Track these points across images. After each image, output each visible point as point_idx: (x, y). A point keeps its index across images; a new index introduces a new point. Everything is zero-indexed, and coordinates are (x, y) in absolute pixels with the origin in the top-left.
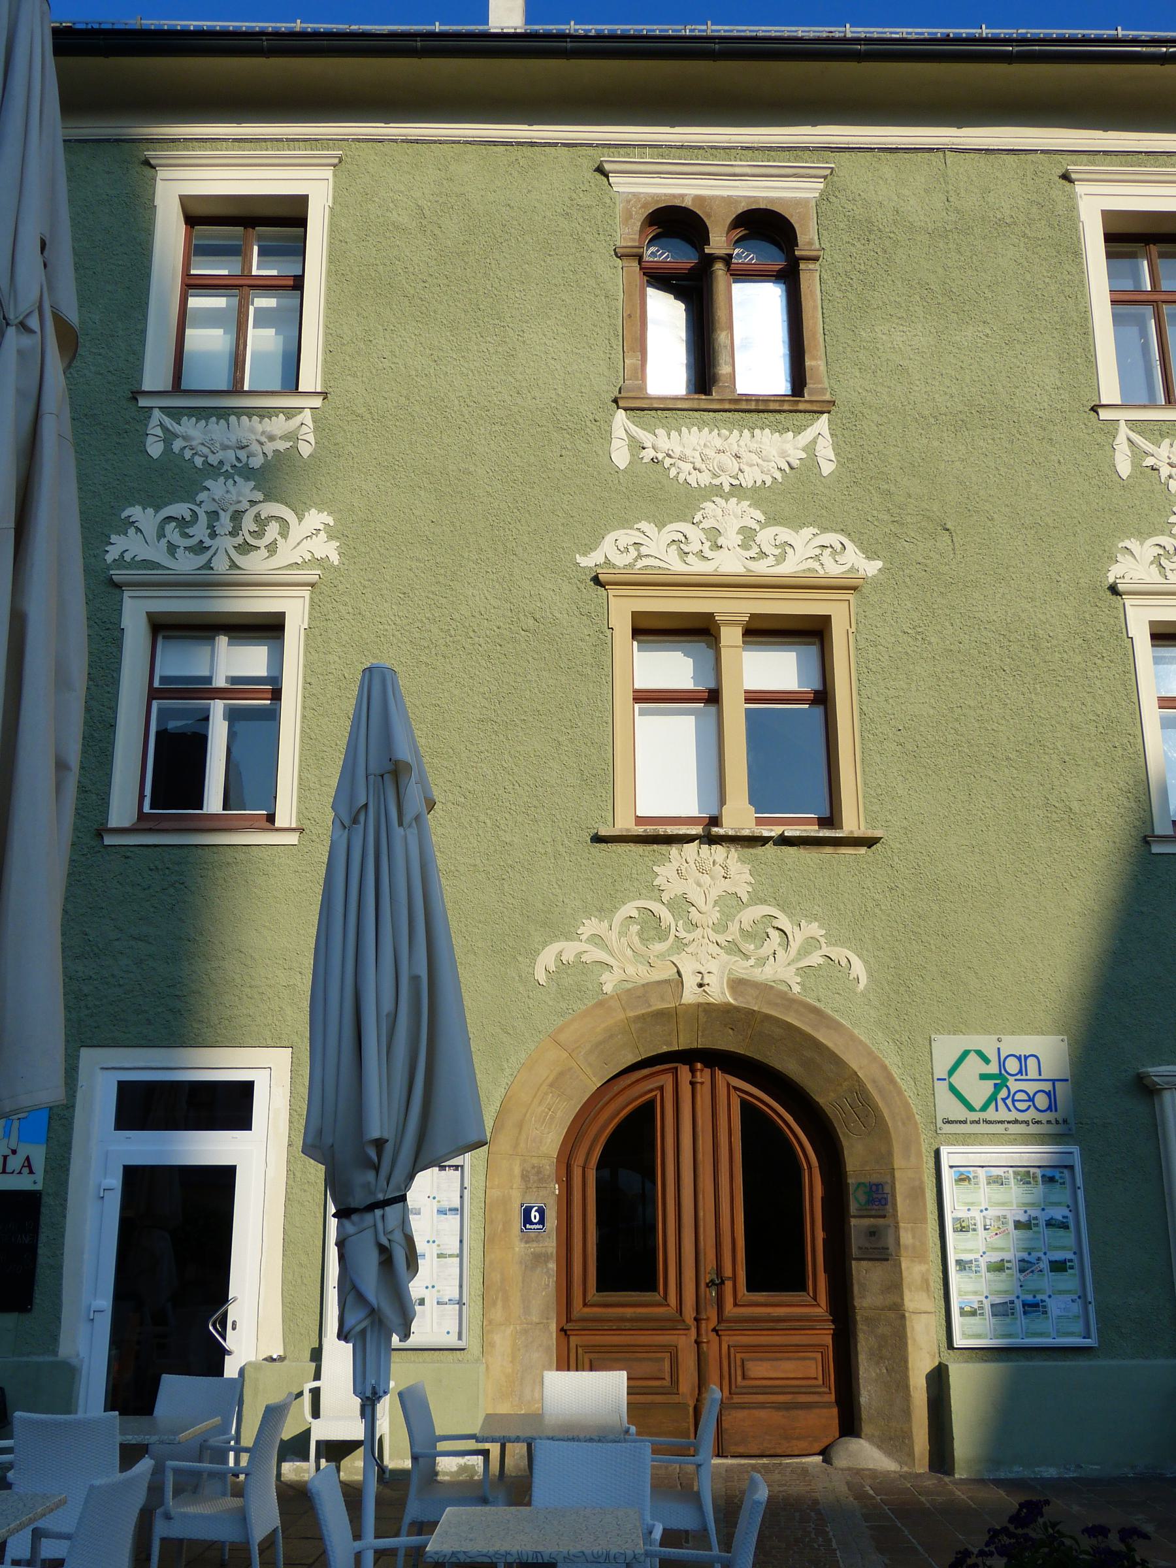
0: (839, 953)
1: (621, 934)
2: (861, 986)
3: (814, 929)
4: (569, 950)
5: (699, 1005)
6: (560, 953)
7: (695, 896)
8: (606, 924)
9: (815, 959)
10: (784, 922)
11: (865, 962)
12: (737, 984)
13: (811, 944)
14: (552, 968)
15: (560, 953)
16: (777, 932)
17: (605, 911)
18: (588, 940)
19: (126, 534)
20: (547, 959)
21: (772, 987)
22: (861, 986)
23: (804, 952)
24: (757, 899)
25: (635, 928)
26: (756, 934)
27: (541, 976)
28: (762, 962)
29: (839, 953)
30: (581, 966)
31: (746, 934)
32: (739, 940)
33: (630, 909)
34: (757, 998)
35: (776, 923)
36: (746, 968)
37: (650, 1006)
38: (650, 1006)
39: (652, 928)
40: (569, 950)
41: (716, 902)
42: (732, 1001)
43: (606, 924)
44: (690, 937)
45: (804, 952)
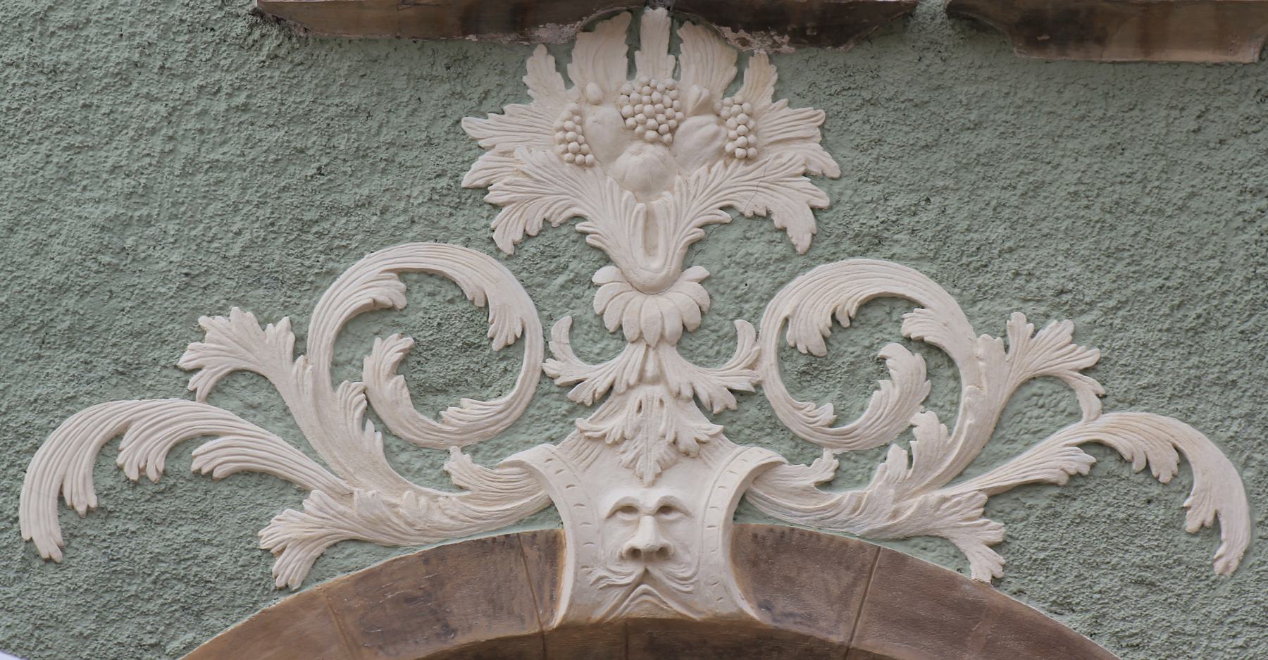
0: (1142, 432)
1: (340, 368)
2: (1228, 552)
3: (1055, 345)
4: (148, 425)
5: (630, 629)
6: (112, 442)
7: (608, 215)
8: (280, 331)
9: (1053, 455)
10: (938, 314)
11: (1231, 447)
12: (763, 547)
13: (1039, 399)
14: (84, 498)
15: (112, 442)
16: (916, 361)
17: (284, 287)
18: (217, 392)
19: (521, 94)
20: (58, 467)
21: (898, 561)
22: (1228, 552)
23: (1005, 431)
24: (836, 237)
25: (388, 348)
26: (835, 360)
27: (39, 525)
28: (857, 462)
29: (1142, 432)
30: (180, 482)
31: (806, 370)
32: (776, 390)
33: (363, 280)
34: (844, 599)
35: (913, 325)
36: (804, 492)
37: (449, 631)
38: (449, 631)
39: (449, 349)
40: (148, 425)
41: (693, 249)
42: (751, 611)
43: (280, 331)
44: (597, 377)
45: (1005, 431)
